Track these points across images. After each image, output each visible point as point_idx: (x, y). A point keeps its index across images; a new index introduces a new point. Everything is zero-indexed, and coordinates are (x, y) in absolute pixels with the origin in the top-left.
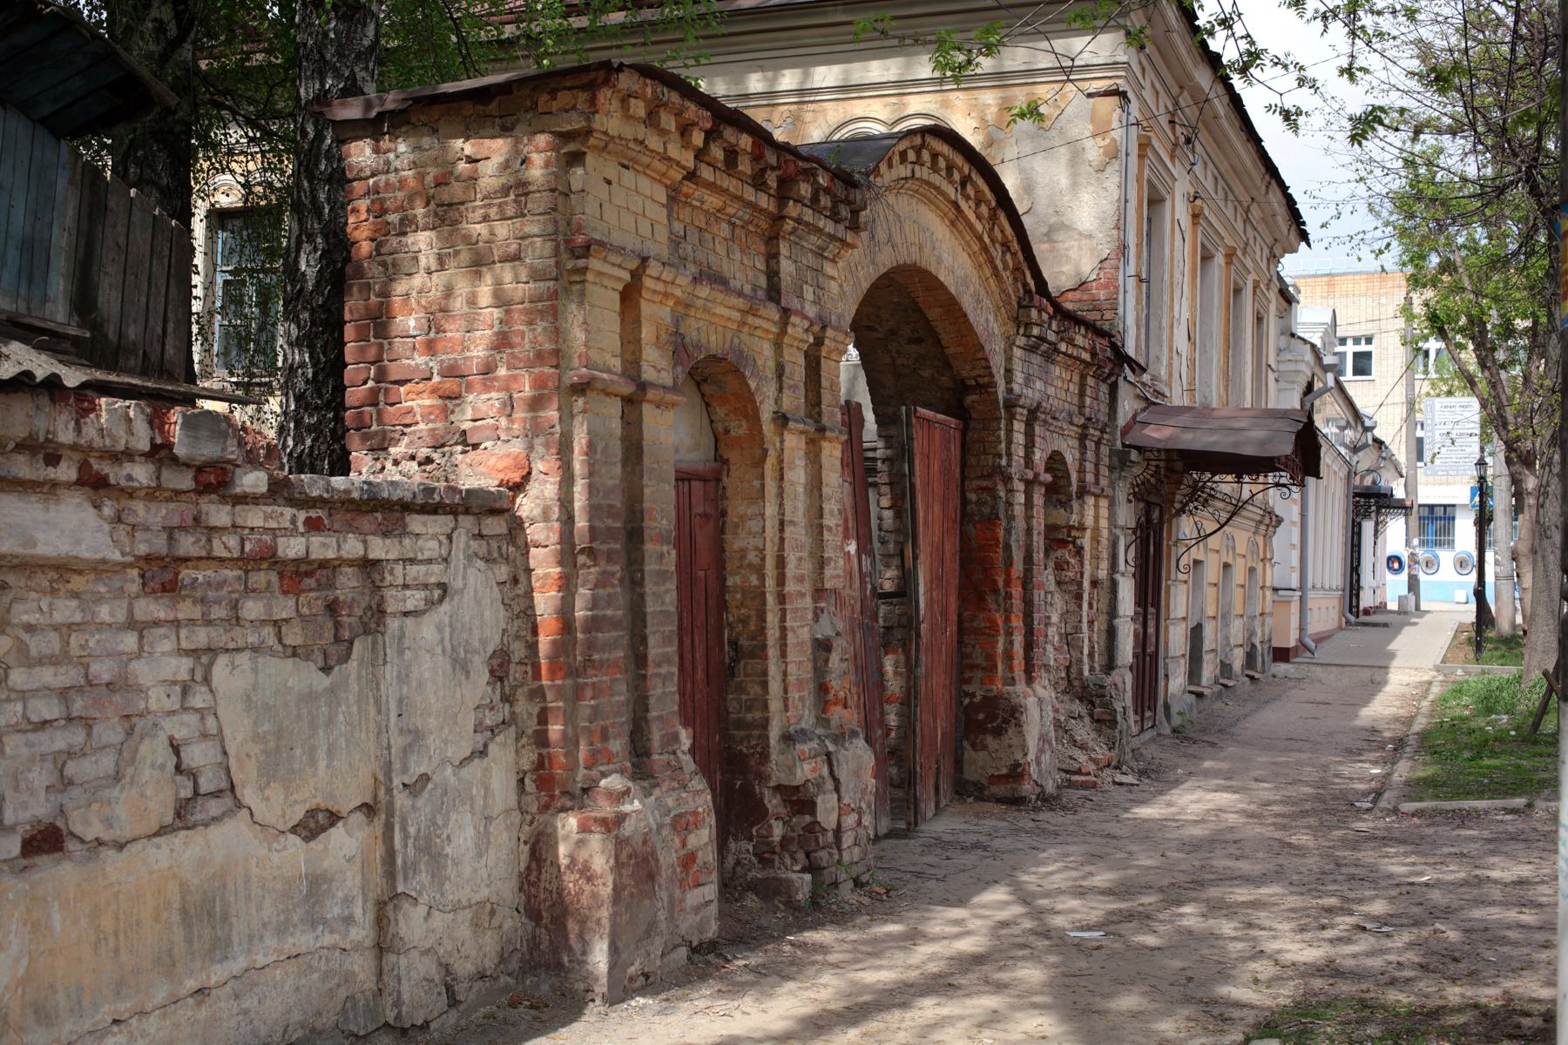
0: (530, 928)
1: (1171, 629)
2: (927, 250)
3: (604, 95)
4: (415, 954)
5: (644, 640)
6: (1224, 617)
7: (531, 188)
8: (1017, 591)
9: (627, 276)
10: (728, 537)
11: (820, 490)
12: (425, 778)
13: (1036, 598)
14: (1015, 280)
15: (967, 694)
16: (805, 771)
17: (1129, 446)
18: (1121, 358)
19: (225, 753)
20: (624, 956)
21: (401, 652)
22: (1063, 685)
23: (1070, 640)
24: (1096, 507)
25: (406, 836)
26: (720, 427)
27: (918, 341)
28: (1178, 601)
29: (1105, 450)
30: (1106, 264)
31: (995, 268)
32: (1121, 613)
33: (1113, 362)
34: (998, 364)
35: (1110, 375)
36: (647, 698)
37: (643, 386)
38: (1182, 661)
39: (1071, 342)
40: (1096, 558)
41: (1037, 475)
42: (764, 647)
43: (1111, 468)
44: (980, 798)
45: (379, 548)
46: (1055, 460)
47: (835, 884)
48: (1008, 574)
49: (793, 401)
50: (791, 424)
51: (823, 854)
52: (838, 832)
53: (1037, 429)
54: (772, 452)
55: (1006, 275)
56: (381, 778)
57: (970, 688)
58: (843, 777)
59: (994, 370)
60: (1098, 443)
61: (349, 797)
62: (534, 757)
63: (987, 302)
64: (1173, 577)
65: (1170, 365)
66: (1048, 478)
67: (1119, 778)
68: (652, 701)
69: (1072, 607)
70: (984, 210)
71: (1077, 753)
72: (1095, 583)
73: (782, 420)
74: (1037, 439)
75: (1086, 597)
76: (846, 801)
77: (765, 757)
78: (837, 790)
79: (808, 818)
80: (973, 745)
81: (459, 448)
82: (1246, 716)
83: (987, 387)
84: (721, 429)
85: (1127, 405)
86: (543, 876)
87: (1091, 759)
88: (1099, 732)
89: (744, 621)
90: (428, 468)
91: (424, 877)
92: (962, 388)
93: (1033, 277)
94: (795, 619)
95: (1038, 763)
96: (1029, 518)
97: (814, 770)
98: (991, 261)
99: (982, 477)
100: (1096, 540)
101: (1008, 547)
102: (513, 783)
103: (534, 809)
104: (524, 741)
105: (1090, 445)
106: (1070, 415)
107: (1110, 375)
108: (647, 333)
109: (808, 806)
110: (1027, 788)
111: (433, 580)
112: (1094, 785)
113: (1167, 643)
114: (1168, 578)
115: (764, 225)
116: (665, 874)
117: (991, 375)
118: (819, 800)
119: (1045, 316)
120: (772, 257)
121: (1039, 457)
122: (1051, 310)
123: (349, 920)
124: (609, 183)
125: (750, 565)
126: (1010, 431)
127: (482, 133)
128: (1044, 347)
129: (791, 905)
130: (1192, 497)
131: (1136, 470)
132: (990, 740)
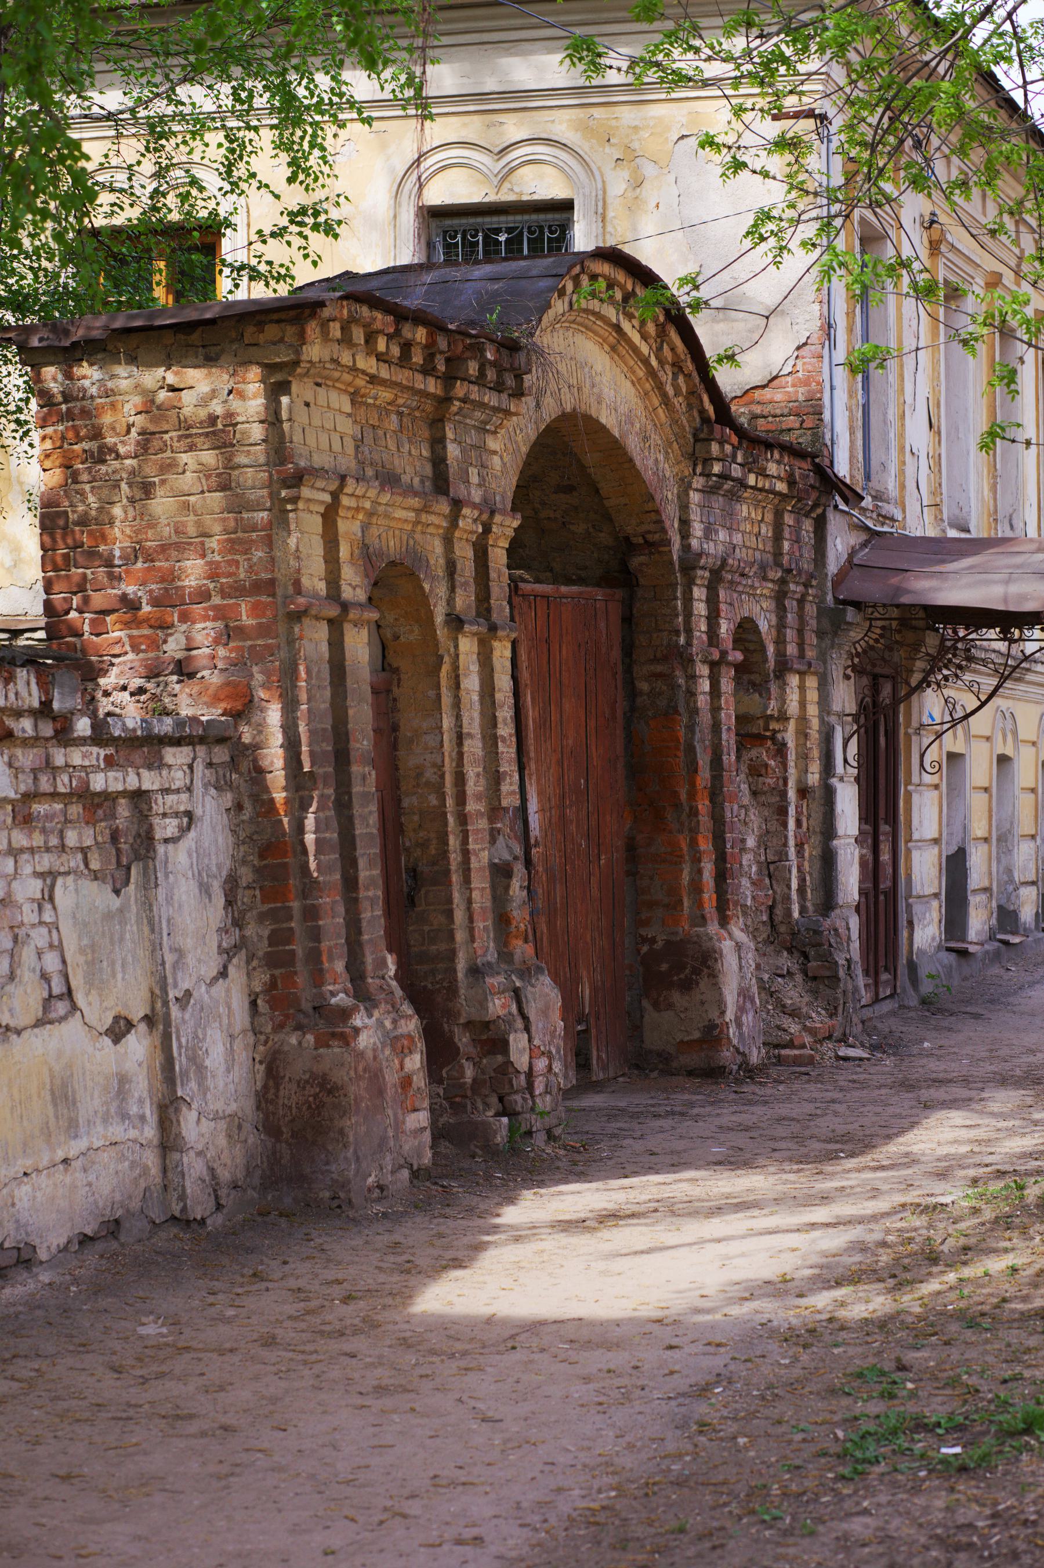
0: (269, 1145)
1: (916, 855)
2: (586, 390)
3: (312, 329)
4: (192, 1153)
5: (354, 863)
6: (1002, 840)
7: (239, 419)
8: (703, 805)
9: (327, 498)
10: (401, 753)
11: (493, 696)
12: (188, 994)
13: (728, 814)
14: (690, 406)
15: (645, 940)
16: (498, 1006)
17: (845, 602)
18: (828, 483)
19: (64, 962)
20: (364, 1165)
21: (167, 876)
22: (765, 932)
23: (772, 870)
24: (802, 688)
25: (180, 1046)
26: (388, 634)
27: (570, 489)
28: (925, 814)
29: (811, 610)
30: (804, 352)
31: (664, 395)
32: (840, 832)
33: (820, 488)
34: (671, 514)
35: (815, 506)
36: (359, 921)
37: (345, 606)
38: (935, 904)
39: (762, 473)
40: (804, 757)
41: (724, 653)
42: (447, 872)
43: (820, 634)
44: (668, 1072)
45: (149, 781)
46: (746, 629)
47: (529, 1133)
48: (693, 784)
49: (465, 600)
50: (467, 628)
51: (518, 1097)
52: (530, 1074)
53: (722, 594)
54: (446, 659)
55: (679, 402)
56: (157, 992)
57: (648, 932)
58: (532, 1016)
59: (667, 524)
60: (801, 601)
61: (137, 1011)
62: (267, 978)
63: (655, 438)
64: (915, 779)
65: (902, 472)
66: (739, 656)
67: (843, 1052)
68: (364, 924)
69: (774, 826)
70: (651, 328)
71: (787, 1022)
72: (803, 792)
73: (456, 623)
74: (723, 607)
75: (792, 811)
76: (536, 1042)
77: (452, 990)
78: (527, 1029)
79: (500, 1058)
80: (656, 1005)
81: (175, 678)
82: (1032, 985)
83: (657, 545)
84: (389, 636)
85: (840, 543)
86: (281, 1093)
87: (805, 1028)
88: (815, 993)
89: (424, 845)
90: (143, 698)
91: (193, 1085)
92: (627, 546)
93: (711, 401)
94: (476, 841)
95: (739, 1025)
96: (715, 709)
97: (503, 1006)
98: (660, 387)
99: (655, 660)
100: (803, 734)
101: (691, 749)
102: (247, 1005)
103: (269, 1029)
104: (255, 963)
105: (791, 604)
106: (763, 567)
107: (815, 506)
108: (344, 552)
109: (501, 1045)
110: (726, 1055)
111: (182, 808)
112: (811, 1061)
113: (909, 876)
114: (908, 782)
115: (429, 408)
116: (390, 1092)
117: (664, 531)
118: (511, 1038)
119: (728, 448)
120: (438, 442)
121: (725, 628)
122: (735, 439)
123: (142, 1118)
124: (307, 405)
125: (427, 784)
126: (688, 600)
127: (184, 362)
128: (728, 485)
129: (492, 1152)
130: (936, 663)
131: (855, 634)
132: (676, 997)
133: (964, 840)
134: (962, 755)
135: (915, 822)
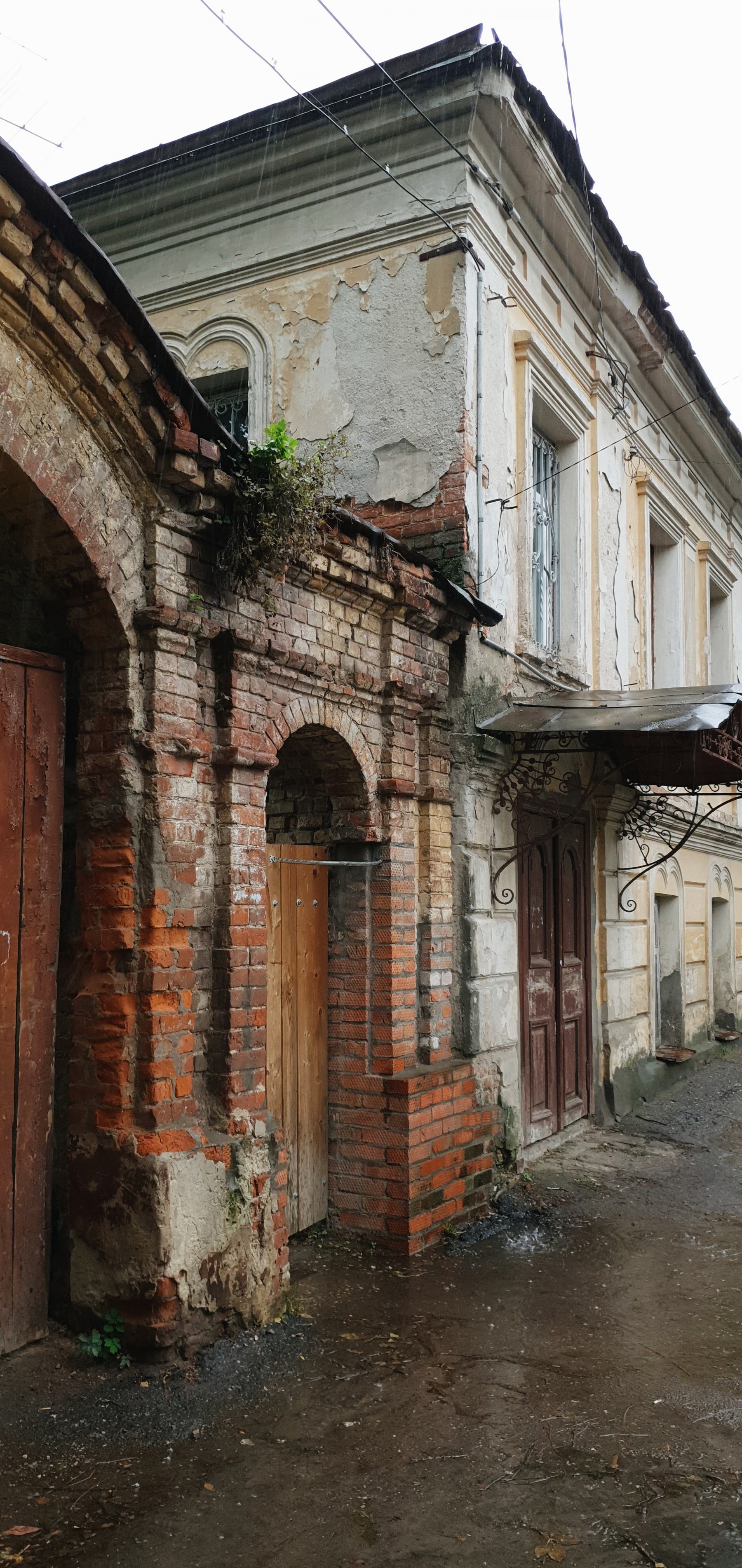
1: (613, 985)
133: (678, 964)
134: (673, 898)
135: (611, 953)
